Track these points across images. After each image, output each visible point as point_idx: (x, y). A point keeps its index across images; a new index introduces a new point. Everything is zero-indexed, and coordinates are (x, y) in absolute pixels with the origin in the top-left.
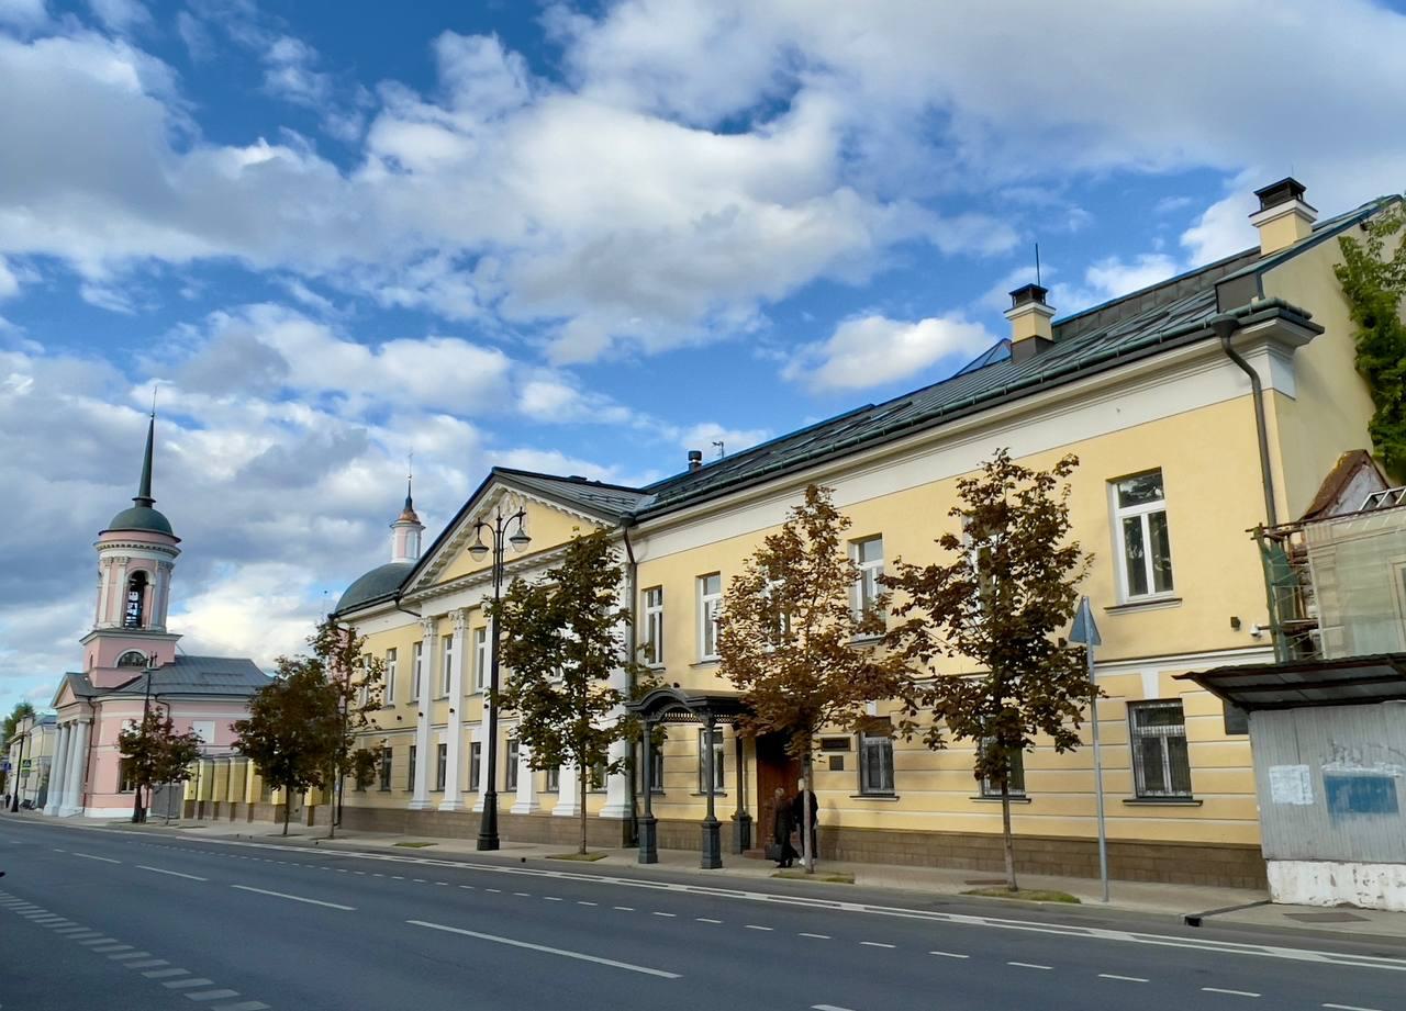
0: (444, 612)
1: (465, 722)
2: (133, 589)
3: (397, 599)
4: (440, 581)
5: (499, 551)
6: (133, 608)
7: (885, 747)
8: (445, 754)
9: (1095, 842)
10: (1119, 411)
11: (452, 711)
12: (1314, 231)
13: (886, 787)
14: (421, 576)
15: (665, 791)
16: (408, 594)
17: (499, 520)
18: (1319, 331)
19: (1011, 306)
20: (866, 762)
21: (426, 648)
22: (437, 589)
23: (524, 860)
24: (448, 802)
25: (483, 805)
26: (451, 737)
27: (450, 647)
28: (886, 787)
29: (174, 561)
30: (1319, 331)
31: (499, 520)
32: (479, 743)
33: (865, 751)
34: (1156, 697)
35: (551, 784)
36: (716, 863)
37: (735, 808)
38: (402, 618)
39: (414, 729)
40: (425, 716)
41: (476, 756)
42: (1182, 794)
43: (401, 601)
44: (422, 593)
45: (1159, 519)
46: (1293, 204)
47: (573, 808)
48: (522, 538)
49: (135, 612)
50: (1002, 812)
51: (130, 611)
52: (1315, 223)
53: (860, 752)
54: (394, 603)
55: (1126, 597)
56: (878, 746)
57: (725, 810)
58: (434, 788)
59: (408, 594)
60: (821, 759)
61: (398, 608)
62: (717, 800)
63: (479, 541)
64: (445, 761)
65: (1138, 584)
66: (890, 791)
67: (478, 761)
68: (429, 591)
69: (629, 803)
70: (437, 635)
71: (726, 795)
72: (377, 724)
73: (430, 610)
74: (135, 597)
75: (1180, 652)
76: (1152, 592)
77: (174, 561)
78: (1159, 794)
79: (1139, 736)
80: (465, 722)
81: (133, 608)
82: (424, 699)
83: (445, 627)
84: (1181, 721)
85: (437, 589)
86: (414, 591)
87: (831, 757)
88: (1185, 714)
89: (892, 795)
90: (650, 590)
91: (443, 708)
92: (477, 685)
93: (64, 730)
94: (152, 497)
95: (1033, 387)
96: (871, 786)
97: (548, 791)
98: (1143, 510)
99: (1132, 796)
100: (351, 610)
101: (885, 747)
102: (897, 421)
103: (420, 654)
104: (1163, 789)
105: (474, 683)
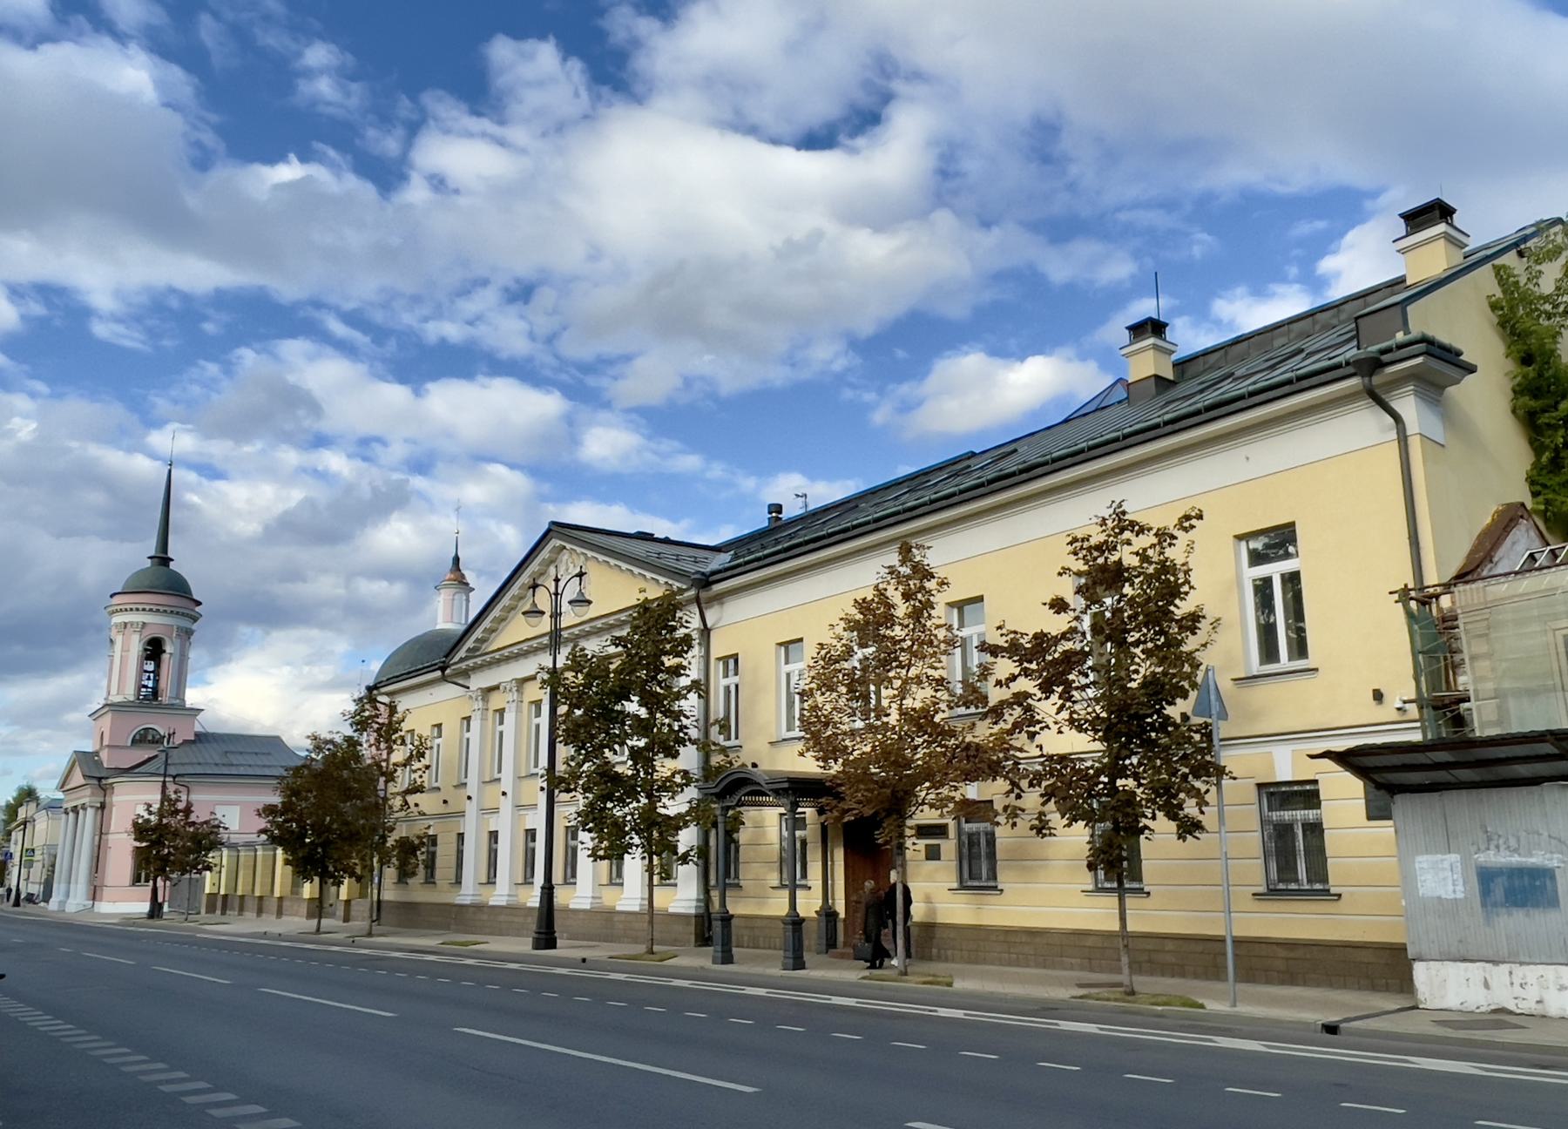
2: (148, 658)
5: (556, 615)
6: (149, 679)
8: (496, 842)
9: (1222, 940)
11: (504, 794)
13: (988, 879)
14: (470, 643)
15: (742, 883)
16: (453, 664)
19: (1128, 342)
20: (965, 851)
22: (487, 658)
25: (538, 899)
26: (503, 823)
27: (501, 723)
28: (988, 879)
31: (557, 580)
32: (535, 830)
34: (1289, 778)
37: (820, 902)
38: (448, 691)
40: (474, 798)
41: (531, 845)
42: (1318, 886)
43: (448, 671)
44: (470, 663)
45: (1292, 579)
49: (150, 684)
51: (146, 683)
54: (439, 673)
56: (979, 834)
61: (444, 679)
62: (799, 893)
63: (534, 604)
64: (496, 850)
65: (1269, 651)
66: (992, 884)
68: (479, 661)
69: (702, 897)
70: (487, 709)
73: (479, 681)
74: (150, 666)
77: (194, 627)
78: (1293, 886)
81: (149, 679)
83: (497, 701)
84: (1318, 805)
85: (487, 658)
86: (462, 660)
87: (926, 845)
89: (995, 888)
90: (725, 659)
91: (494, 790)
93: (71, 814)
94: (170, 555)
96: (971, 877)
100: (390, 681)
102: (1001, 470)
103: (468, 730)
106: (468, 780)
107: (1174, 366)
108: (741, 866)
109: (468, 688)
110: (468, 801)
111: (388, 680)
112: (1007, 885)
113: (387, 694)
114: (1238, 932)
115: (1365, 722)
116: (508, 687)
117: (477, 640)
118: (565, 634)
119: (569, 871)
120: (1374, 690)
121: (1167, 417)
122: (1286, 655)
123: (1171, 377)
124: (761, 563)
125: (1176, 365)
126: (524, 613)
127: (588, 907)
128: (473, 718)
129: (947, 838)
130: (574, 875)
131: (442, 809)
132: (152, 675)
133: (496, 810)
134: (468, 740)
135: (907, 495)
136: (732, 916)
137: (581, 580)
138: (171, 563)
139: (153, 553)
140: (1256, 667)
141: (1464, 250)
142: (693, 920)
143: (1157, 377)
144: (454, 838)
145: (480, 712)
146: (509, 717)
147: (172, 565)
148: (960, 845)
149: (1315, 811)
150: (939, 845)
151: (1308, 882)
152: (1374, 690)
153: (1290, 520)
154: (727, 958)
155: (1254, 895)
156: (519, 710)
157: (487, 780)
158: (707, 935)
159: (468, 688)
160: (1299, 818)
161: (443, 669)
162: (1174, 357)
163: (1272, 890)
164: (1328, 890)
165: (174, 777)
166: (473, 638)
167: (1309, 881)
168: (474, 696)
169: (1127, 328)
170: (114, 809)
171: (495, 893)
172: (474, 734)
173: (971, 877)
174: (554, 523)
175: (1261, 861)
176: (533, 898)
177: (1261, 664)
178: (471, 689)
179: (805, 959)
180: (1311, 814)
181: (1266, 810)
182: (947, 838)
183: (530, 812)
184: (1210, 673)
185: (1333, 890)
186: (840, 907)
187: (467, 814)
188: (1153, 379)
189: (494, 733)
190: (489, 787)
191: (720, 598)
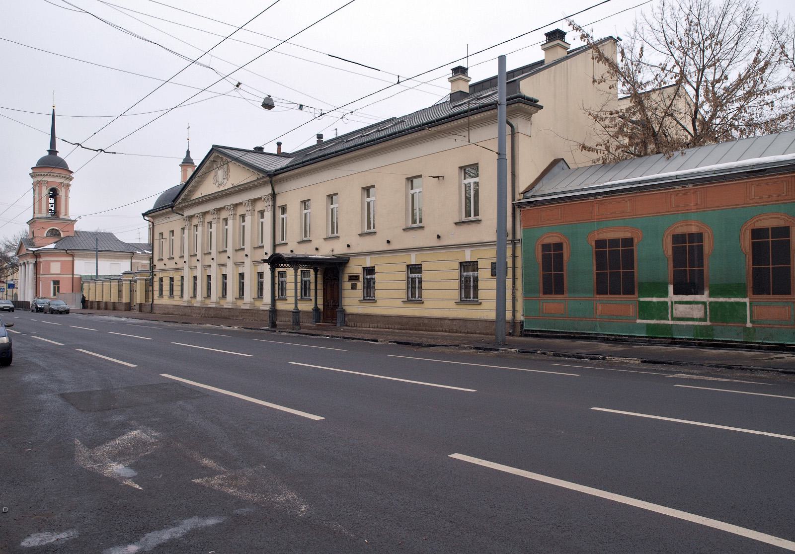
1: (205, 266)
2: (51, 197)
3: (172, 207)
4: (192, 199)
6: (52, 206)
7: (419, 278)
8: (226, 279)
12: (568, 54)
14: (182, 196)
16: (177, 205)
18: (541, 107)
20: (410, 285)
22: (190, 203)
26: (198, 273)
27: (226, 225)
28: (474, 298)
29: (71, 183)
30: (541, 107)
32: (243, 273)
34: (414, 264)
35: (280, 295)
40: (215, 259)
41: (225, 281)
43: (174, 208)
44: (183, 205)
45: (477, 184)
46: (559, 42)
49: (53, 209)
51: (51, 208)
52: (569, 50)
53: (408, 280)
54: (170, 209)
56: (470, 277)
58: (221, 296)
60: (347, 285)
61: (173, 211)
64: (226, 284)
66: (420, 299)
68: (186, 204)
71: (423, 302)
73: (188, 213)
74: (52, 201)
75: (476, 242)
77: (71, 183)
81: (52, 206)
82: (230, 249)
88: (423, 269)
93: (23, 267)
94: (57, 150)
98: (471, 181)
99: (459, 300)
101: (419, 278)
103: (197, 231)
105: (240, 244)
106: (228, 249)
107: (469, 87)
108: (294, 288)
110: (228, 259)
116: (266, 199)
117: (185, 195)
119: (241, 293)
121: (320, 154)
123: (468, 92)
125: (470, 86)
128: (213, 223)
129: (359, 281)
130: (243, 295)
131: (175, 266)
132: (53, 205)
133: (242, 263)
134: (211, 232)
138: (58, 153)
139: (49, 149)
144: (180, 279)
146: (230, 222)
147: (58, 155)
150: (356, 284)
157: (256, 246)
161: (172, 207)
162: (470, 83)
165: (66, 251)
166: (184, 194)
169: (545, 34)
170: (41, 264)
172: (186, 235)
174: (214, 146)
182: (359, 281)
186: (321, 307)
189: (223, 230)
190: (207, 256)
191: (281, 181)
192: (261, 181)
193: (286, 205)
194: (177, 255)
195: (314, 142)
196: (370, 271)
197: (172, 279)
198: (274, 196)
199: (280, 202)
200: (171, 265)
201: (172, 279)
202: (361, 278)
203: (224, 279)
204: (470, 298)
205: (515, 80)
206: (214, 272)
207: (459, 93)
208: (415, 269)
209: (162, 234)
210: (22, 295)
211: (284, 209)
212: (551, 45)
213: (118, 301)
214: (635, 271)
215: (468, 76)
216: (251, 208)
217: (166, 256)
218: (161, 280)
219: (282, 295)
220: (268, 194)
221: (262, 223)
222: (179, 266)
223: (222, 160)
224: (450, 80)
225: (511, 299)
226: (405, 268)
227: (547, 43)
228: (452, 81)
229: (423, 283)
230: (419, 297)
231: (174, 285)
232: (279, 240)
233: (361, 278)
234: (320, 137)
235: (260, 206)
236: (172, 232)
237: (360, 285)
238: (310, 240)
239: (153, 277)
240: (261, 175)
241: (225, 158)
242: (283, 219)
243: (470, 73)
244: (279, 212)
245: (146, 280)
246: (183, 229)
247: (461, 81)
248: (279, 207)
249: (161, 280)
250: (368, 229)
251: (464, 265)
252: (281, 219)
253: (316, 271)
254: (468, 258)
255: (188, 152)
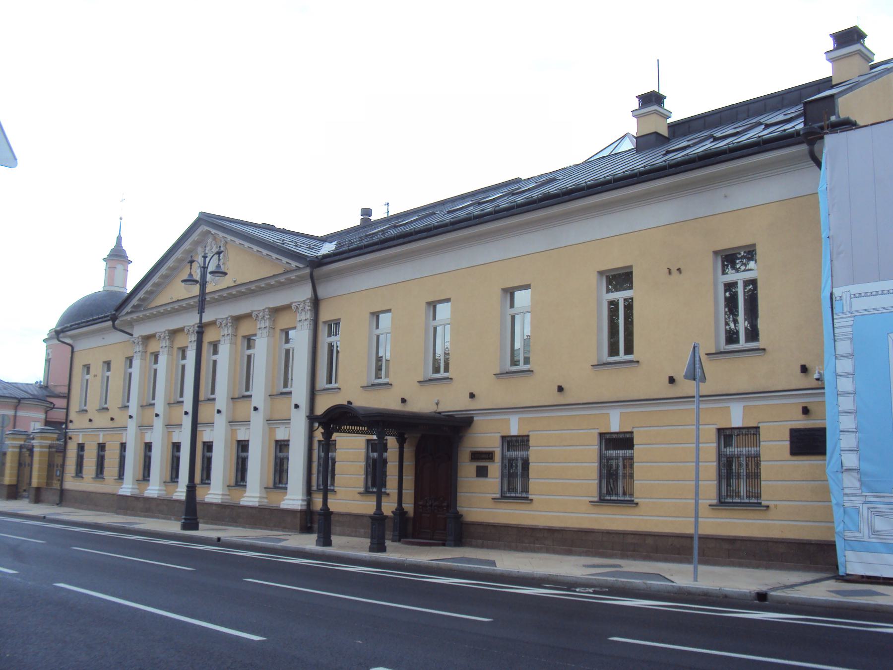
0: (248, 311)
3: (114, 318)
5: (203, 284)
8: (125, 451)
9: (690, 537)
10: (726, 196)
11: (219, 412)
13: (624, 494)
14: (135, 302)
15: (336, 489)
17: (205, 257)
19: (638, 108)
21: (136, 363)
22: (148, 313)
23: (219, 539)
24: (154, 490)
25: (185, 494)
26: (157, 437)
27: (131, 366)
28: (522, 492)
31: (205, 257)
33: (506, 462)
36: (383, 549)
37: (396, 505)
38: (118, 337)
39: (125, 428)
40: (293, 406)
42: (753, 500)
43: (116, 322)
44: (134, 316)
45: (629, 306)
46: (655, 107)
47: (300, 502)
48: (220, 273)
50: (413, 501)
54: (110, 323)
55: (723, 346)
56: (517, 460)
57: (389, 507)
58: (141, 478)
59: (123, 316)
60: (467, 469)
62: (330, 496)
63: (191, 275)
65: (613, 350)
66: (524, 495)
67: (178, 458)
68: (141, 315)
69: (305, 498)
70: (146, 352)
72: (679, 375)
73: (140, 331)
75: (500, 407)
76: (742, 344)
78: (737, 500)
79: (725, 455)
80: (168, 426)
83: (153, 346)
84: (757, 443)
85: (148, 313)
86: (128, 313)
87: (478, 467)
89: (527, 498)
90: (329, 324)
91: (149, 412)
92: (83, 405)
95: (371, 248)
96: (509, 490)
97: (275, 487)
98: (620, 296)
100: (71, 328)
101: (522, 459)
102: (482, 210)
103: (377, 327)
104: (739, 497)
109: (131, 335)
111: (71, 326)
112: (643, 500)
113: (71, 337)
114: (701, 532)
115: (652, 397)
118: (208, 298)
120: (402, 399)
122: (443, 370)
124: (362, 251)
126: (183, 281)
127: (220, 501)
128: (161, 353)
130: (149, 475)
135: (472, 208)
136: (332, 513)
137: (191, 265)
140: (607, 359)
141: (870, 64)
142: (299, 515)
143: (656, 133)
144: (118, 447)
145: (140, 354)
146: (163, 359)
148: (503, 467)
149: (630, 451)
150: (487, 467)
151: (747, 497)
152: (402, 399)
153: (752, 242)
154: (327, 542)
155: (710, 505)
156: (170, 354)
158: (309, 525)
159: (131, 335)
160: (744, 452)
162: (669, 121)
163: (602, 500)
164: (760, 503)
167: (748, 497)
168: (136, 341)
169: (637, 97)
171: (210, 492)
172: (136, 370)
173: (509, 490)
175: (715, 483)
176: (180, 493)
177: (433, 373)
178: (134, 336)
179: (386, 544)
180: (627, 453)
181: (603, 450)
183: (177, 431)
184: (696, 349)
185: (764, 503)
187: (215, 424)
188: (653, 137)
191: (328, 277)
192: (293, 276)
193: (340, 319)
194: (114, 403)
195: (355, 220)
196: (519, 442)
197: (102, 447)
198: (316, 302)
199: (326, 315)
200: (101, 420)
201: (102, 447)
202: (498, 457)
203: (148, 449)
204: (516, 492)
205: (832, 97)
206: (131, 438)
207: (653, 137)
208: (624, 441)
209: (87, 368)
210: (702, 407)
211: (334, 326)
212: (849, 51)
213: (45, 487)
214: (85, 454)
215: (665, 108)
216: (267, 324)
217: (93, 403)
218: (81, 447)
219: (280, 482)
220: (165, 330)
221: (215, 362)
222: (118, 423)
223: (215, 239)
224: (636, 113)
225: (390, 326)
226: (596, 440)
227: (835, 49)
228: (636, 114)
229: (337, 464)
230: (522, 492)
231: (106, 457)
232: (322, 381)
233: (498, 457)
234: (366, 212)
235: (180, 341)
236: (108, 364)
237: (495, 469)
238: (387, 384)
239: (66, 443)
240: (294, 264)
241: (221, 234)
242: (331, 346)
243: (667, 104)
244: (323, 331)
245: (50, 447)
246: (130, 360)
247: (655, 114)
248: (324, 323)
249: (81, 447)
250: (327, 384)
251: (726, 435)
252: (212, 362)
253: (401, 442)
254: (514, 431)
255: (119, 239)
